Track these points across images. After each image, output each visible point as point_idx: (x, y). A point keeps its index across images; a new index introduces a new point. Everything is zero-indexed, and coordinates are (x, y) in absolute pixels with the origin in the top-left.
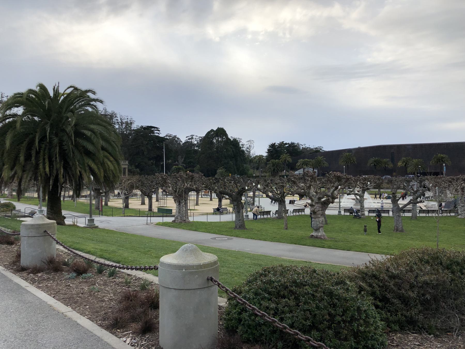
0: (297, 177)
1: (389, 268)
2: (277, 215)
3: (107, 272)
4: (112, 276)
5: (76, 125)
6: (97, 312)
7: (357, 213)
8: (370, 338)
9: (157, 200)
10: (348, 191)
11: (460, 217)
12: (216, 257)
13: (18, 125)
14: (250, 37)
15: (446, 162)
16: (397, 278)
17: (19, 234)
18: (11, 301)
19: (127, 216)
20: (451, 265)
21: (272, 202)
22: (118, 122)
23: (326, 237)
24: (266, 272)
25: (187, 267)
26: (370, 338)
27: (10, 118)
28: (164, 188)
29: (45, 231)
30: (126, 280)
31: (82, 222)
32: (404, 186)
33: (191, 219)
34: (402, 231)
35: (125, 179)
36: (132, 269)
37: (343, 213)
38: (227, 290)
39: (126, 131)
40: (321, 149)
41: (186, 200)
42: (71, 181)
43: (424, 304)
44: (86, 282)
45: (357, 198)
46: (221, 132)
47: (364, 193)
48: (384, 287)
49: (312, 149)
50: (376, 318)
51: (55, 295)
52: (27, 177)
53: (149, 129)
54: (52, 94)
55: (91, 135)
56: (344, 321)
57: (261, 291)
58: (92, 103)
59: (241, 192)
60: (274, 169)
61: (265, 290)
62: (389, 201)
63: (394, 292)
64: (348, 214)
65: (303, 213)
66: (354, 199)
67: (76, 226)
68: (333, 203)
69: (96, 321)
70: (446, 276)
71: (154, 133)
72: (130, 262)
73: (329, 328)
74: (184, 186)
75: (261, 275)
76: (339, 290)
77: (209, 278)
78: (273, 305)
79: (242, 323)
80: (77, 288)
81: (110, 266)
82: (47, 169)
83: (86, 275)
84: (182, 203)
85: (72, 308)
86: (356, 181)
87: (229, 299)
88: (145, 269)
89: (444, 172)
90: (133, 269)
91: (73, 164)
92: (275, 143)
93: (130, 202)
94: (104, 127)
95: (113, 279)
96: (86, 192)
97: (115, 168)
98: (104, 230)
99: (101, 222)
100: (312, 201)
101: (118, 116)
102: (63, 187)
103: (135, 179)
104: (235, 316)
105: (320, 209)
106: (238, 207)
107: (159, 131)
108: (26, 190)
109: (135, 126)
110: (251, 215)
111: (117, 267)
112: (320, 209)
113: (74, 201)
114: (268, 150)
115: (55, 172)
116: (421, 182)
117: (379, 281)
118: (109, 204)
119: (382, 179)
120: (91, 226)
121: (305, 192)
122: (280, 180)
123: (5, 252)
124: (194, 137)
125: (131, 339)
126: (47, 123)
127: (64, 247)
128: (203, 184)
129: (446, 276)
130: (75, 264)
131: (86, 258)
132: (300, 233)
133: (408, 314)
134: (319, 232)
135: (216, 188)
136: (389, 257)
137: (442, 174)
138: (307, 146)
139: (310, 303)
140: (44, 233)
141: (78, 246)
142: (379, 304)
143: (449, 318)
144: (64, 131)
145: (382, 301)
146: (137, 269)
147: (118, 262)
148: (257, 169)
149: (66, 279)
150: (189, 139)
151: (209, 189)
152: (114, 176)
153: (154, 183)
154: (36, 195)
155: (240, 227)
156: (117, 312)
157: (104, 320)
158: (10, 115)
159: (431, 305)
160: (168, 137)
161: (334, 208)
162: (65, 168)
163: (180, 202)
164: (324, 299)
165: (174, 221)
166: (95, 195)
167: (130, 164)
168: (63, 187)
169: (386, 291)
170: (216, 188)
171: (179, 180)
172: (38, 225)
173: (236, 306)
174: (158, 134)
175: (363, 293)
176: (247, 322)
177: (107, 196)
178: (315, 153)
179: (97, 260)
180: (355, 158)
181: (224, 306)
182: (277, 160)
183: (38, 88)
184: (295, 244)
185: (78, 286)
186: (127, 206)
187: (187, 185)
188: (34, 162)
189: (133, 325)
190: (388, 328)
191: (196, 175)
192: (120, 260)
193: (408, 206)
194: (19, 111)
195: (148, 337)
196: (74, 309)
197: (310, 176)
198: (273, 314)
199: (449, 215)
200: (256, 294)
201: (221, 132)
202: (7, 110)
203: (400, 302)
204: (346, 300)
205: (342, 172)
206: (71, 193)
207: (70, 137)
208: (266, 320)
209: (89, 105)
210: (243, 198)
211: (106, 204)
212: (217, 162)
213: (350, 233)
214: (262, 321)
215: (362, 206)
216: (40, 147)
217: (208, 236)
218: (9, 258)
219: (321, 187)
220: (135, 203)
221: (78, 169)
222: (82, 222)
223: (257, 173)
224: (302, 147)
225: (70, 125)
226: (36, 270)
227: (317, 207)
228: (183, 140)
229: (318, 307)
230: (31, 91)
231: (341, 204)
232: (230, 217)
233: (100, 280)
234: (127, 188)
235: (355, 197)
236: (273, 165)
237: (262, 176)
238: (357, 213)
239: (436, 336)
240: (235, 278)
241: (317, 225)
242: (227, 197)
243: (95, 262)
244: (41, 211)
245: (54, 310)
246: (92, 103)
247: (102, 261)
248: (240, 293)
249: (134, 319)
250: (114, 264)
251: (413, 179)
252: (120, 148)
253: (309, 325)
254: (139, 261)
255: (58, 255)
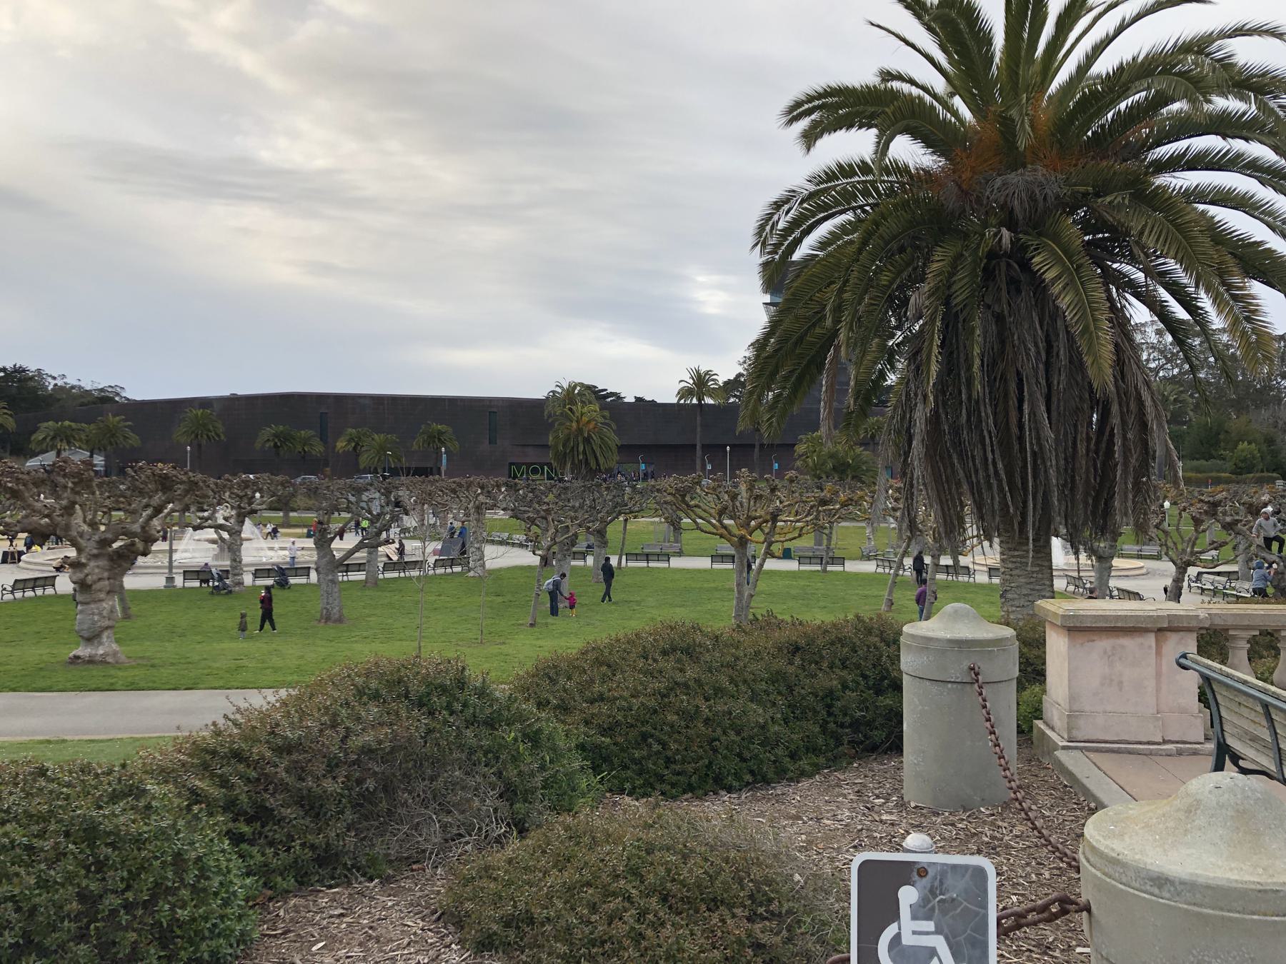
0: (25, 477)
1: (277, 725)
7: (221, 579)
8: (207, 934)
10: (193, 516)
11: (471, 574)
15: (449, 444)
16: (298, 751)
20: (429, 694)
23: (122, 658)
26: (207, 934)
32: (349, 502)
34: (340, 620)
37: (179, 581)
40: (118, 394)
43: (361, 805)
45: (221, 538)
47: (243, 522)
48: (263, 781)
49: (88, 393)
50: (229, 872)
56: (128, 907)
62: (310, 543)
63: (286, 788)
64: (196, 584)
65: (49, 591)
66: (213, 542)
68: (145, 554)
70: (413, 724)
73: (82, 937)
76: (121, 817)
86: (219, 490)
89: (443, 468)
100: (79, 550)
105: (106, 575)
112: (106, 575)
116: (387, 493)
117: (248, 766)
119: (294, 485)
121: (54, 525)
129: (413, 724)
132: (35, 653)
133: (319, 840)
134: (101, 643)
136: (283, 693)
137: (440, 474)
138: (71, 381)
139: (17, 875)
142: (245, 829)
143: (416, 827)
145: (252, 820)
159: (377, 805)
161: (151, 570)
164: (65, 855)
169: (266, 790)
175: (196, 808)
178: (97, 407)
180: (219, 425)
184: (14, 690)
190: (265, 891)
193: (357, 555)
197: (73, 475)
199: (449, 570)
203: (302, 813)
204: (139, 842)
205: (179, 463)
213: (199, 638)
215: (236, 560)
219: (110, 509)
224: (53, 382)
227: (95, 569)
229: (43, 884)
231: (175, 557)
235: (215, 536)
238: (221, 579)
239: (386, 880)
241: (94, 623)
251: (371, 485)
253: (11, 946)
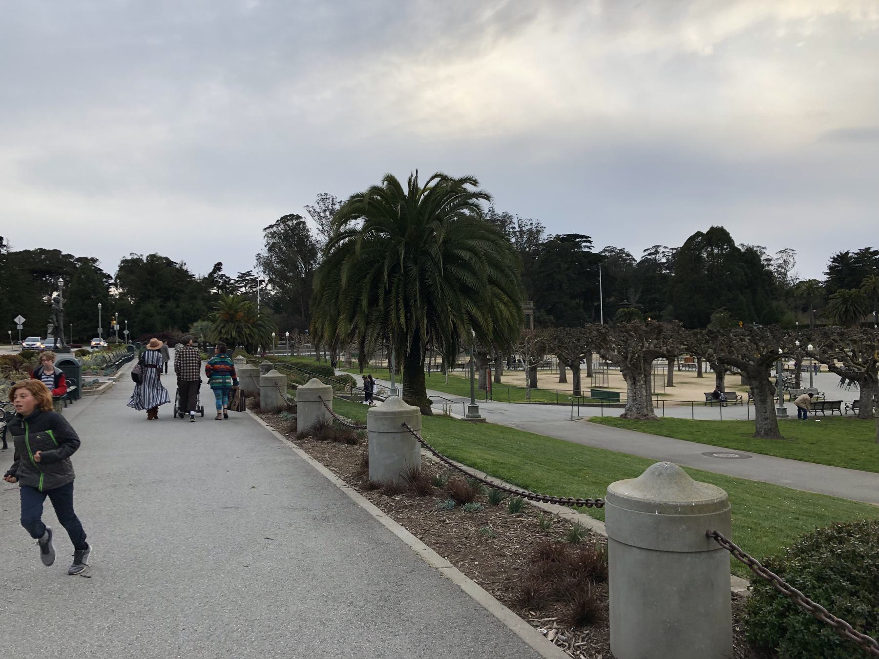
2: (857, 411)
3: (507, 503)
4: (517, 511)
5: (445, 242)
6: (494, 574)
9: (589, 375)
12: (724, 492)
13: (358, 247)
14: (781, 32)
17: (366, 428)
18: (357, 538)
19: (536, 403)
21: (843, 381)
22: (514, 232)
24: (841, 534)
25: (662, 507)
27: (345, 237)
28: (602, 351)
29: (404, 425)
30: (542, 522)
31: (458, 411)
33: (658, 413)
35: (530, 334)
36: (554, 502)
38: (752, 562)
39: (529, 247)
41: (647, 376)
42: (439, 339)
44: (472, 518)
46: (718, 236)
51: (423, 535)
52: (372, 334)
53: (572, 241)
54: (406, 191)
55: (471, 258)
57: (831, 572)
58: (471, 201)
59: (770, 360)
60: (847, 311)
61: (843, 573)
67: (450, 417)
69: (493, 590)
71: (581, 247)
72: (546, 488)
74: (642, 347)
75: (830, 538)
77: (710, 532)
78: (863, 607)
79: (788, 635)
80: (457, 526)
81: (512, 492)
82: (403, 320)
83: (472, 506)
84: (639, 381)
85: (451, 562)
87: (754, 582)
88: (577, 504)
90: (555, 502)
91: (442, 311)
92: (847, 253)
93: (538, 376)
94: (493, 241)
95: (518, 517)
96: (464, 359)
97: (512, 314)
98: (495, 426)
99: (491, 412)
101: (515, 220)
102: (428, 350)
103: (545, 335)
104: (772, 618)
106: (762, 390)
107: (590, 242)
108: (371, 356)
109: (544, 238)
110: (792, 410)
111: (525, 496)
113: (444, 374)
114: (831, 268)
115: (414, 323)
118: (503, 379)
120: (473, 416)
122: (865, 332)
123: (346, 457)
124: (661, 250)
125: (557, 633)
126: (400, 242)
127: (434, 454)
128: (682, 343)
130: (452, 484)
131: (471, 476)
135: (710, 351)
140: (401, 427)
141: (455, 453)
144: (426, 253)
146: (561, 503)
147: (526, 487)
148: (805, 310)
149: (439, 510)
150: (650, 254)
151: (697, 353)
152: (511, 329)
153: (582, 343)
154: (385, 363)
155: (766, 434)
156: (528, 579)
157: (507, 590)
158: (345, 232)
160: (607, 254)
162: (429, 317)
163: (634, 379)
165: (624, 416)
166: (479, 364)
167: (538, 307)
168: (428, 350)
170: (710, 351)
171: (631, 335)
172: (392, 413)
173: (772, 598)
174: (589, 247)
176: (800, 635)
177: (498, 366)
179: (489, 479)
181: (742, 594)
182: (854, 290)
183: (386, 183)
185: (458, 524)
186: (533, 384)
187: (650, 345)
188: (382, 308)
189: (559, 607)
191: (667, 327)
192: (528, 483)
194: (358, 224)
195: (588, 634)
196: (455, 564)
198: (862, 626)
200: (820, 578)
201: (718, 236)
202: (341, 225)
206: (439, 360)
207: (436, 264)
208: (848, 636)
209: (466, 205)
210: (773, 373)
211: (498, 380)
212: (714, 296)
214: (837, 637)
216: (391, 283)
217: (697, 449)
218: (352, 468)
220: (548, 379)
221: (451, 318)
222: (458, 411)
223: (803, 319)
225: (436, 242)
226: (392, 490)
228: (638, 256)
230: (375, 190)
232: (743, 412)
233: (495, 516)
234: (533, 352)
236: (845, 301)
237: (817, 326)
240: (764, 539)
242: (735, 369)
243: (487, 483)
244: (394, 391)
245: (423, 561)
246: (471, 201)
247: (497, 482)
248: (780, 571)
249: (559, 596)
250: (521, 490)
252: (520, 278)
254: (562, 488)
255: (424, 467)
